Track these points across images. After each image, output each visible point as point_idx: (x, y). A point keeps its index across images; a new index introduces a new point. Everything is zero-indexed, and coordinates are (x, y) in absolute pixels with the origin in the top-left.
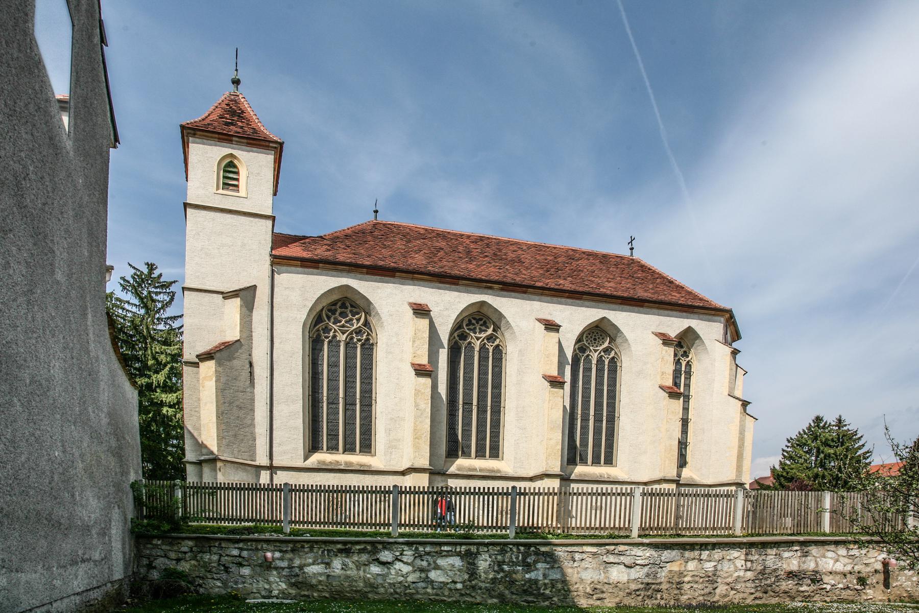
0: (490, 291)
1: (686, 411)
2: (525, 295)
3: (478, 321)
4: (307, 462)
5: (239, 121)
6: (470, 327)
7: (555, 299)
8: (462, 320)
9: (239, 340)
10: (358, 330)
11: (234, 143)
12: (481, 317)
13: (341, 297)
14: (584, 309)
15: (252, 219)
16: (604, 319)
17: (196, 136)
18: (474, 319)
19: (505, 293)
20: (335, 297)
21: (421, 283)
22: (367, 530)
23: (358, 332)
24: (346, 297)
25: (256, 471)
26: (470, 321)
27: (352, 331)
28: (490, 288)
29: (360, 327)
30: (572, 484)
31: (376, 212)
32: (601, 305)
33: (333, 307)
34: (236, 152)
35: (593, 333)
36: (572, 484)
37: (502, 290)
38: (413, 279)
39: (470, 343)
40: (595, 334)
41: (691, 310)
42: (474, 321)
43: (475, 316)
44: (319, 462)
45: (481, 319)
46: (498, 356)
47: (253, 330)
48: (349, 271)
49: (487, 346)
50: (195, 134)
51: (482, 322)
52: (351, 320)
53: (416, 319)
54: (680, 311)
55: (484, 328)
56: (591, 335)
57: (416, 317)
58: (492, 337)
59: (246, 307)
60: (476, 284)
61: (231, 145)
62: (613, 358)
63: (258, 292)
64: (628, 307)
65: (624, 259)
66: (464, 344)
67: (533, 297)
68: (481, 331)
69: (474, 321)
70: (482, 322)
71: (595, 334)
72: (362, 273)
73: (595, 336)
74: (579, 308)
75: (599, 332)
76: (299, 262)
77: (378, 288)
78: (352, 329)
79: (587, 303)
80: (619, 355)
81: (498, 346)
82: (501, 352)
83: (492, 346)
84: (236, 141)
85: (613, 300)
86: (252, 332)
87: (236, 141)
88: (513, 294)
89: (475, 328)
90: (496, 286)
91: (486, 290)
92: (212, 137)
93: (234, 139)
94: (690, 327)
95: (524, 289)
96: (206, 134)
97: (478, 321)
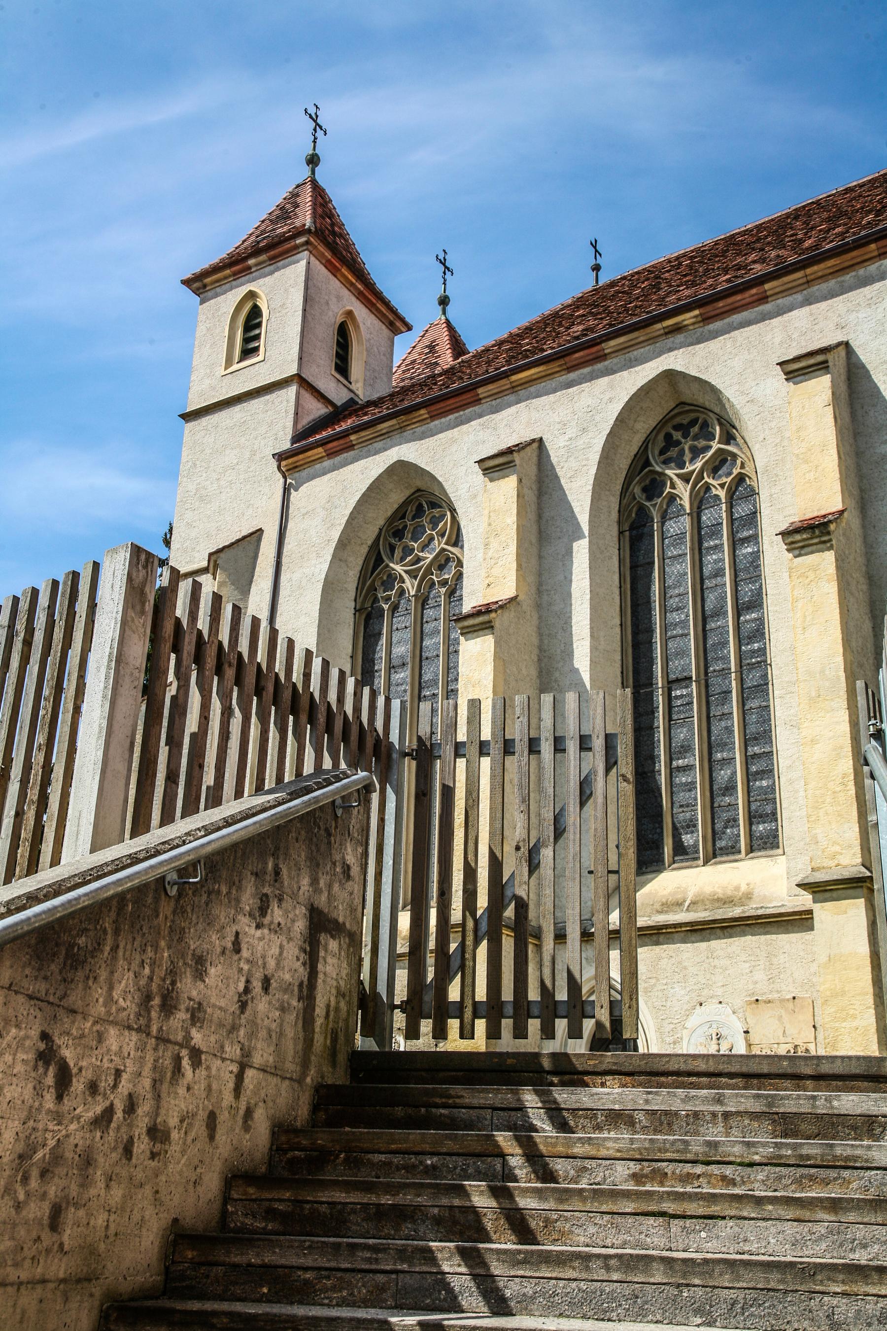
0: (680, 338)
1: (470, 887)
3: (684, 429)
9: (516, 597)
12: (693, 415)
13: (408, 493)
15: (267, 397)
18: (677, 428)
19: (717, 325)
22: (443, 1047)
26: (668, 437)
28: (678, 329)
30: (863, 900)
36: (863, 900)
37: (706, 319)
38: (514, 389)
42: (677, 435)
43: (678, 420)
45: (694, 422)
50: (205, 286)
51: (696, 429)
53: (490, 485)
55: (702, 443)
57: (491, 480)
58: (724, 461)
59: (233, 584)
61: (251, 276)
63: (265, 536)
68: (696, 453)
69: (677, 435)
76: (320, 450)
77: (454, 441)
78: (428, 561)
84: (256, 265)
89: (682, 453)
90: (688, 318)
91: (670, 341)
95: (754, 291)
97: (684, 429)
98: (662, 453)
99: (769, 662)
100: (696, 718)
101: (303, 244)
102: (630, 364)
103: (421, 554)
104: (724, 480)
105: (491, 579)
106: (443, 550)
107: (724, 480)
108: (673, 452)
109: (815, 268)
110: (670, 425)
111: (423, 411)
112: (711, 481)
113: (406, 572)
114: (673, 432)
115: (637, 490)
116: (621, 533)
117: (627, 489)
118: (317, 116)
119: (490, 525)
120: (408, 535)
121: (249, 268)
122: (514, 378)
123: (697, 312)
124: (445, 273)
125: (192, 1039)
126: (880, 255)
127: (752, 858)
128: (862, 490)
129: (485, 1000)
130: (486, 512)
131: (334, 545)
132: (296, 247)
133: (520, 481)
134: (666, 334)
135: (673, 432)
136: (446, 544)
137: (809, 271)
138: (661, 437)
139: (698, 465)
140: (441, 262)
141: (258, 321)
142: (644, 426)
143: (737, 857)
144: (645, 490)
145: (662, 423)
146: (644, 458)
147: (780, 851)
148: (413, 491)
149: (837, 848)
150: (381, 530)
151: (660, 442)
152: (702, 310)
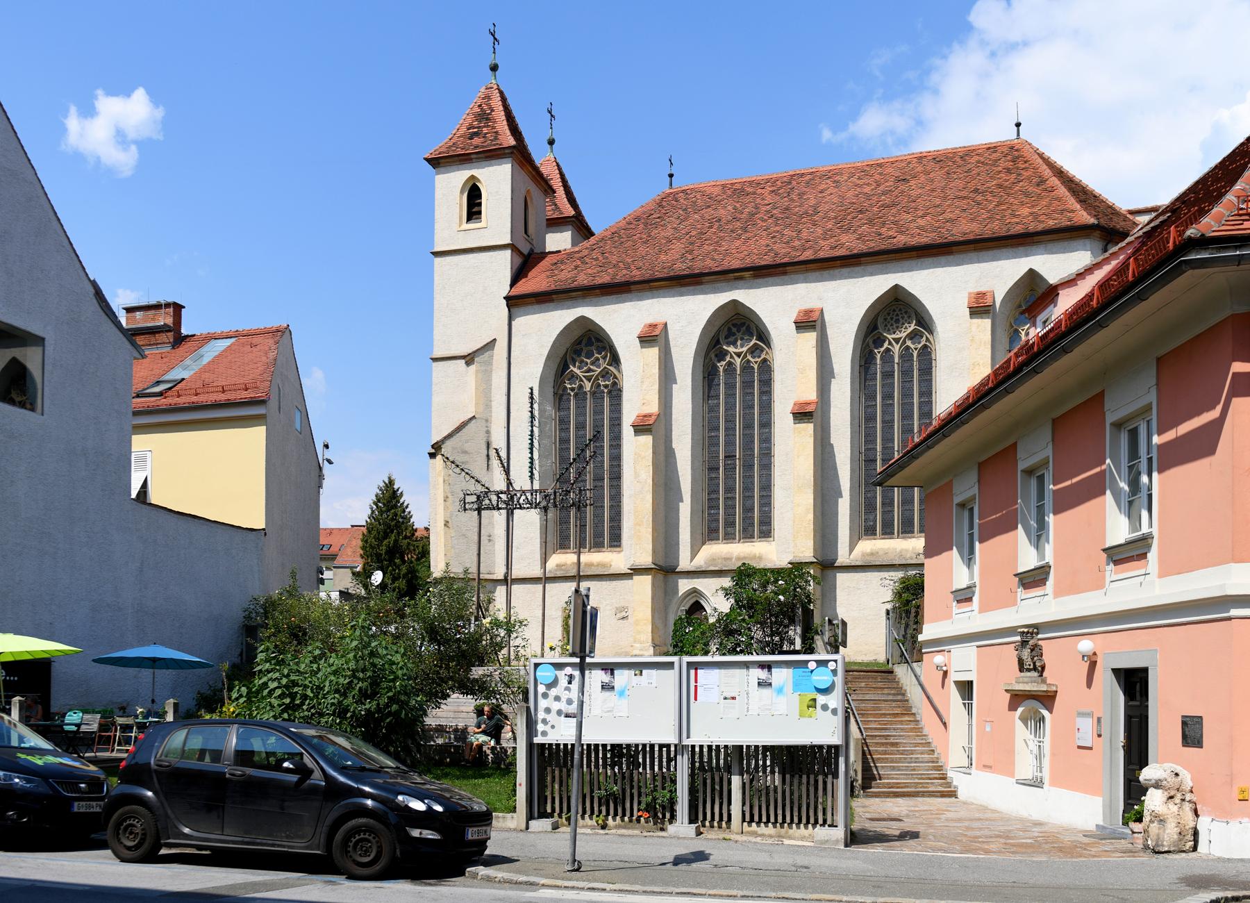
0: (741, 283)
2: (786, 278)
4: (851, 557)
5: (485, 127)
6: (730, 339)
7: (825, 273)
8: (719, 331)
10: (604, 373)
11: (474, 160)
12: (743, 321)
14: (867, 279)
16: (896, 287)
17: (441, 165)
18: (734, 325)
20: (577, 334)
21: (661, 291)
23: (605, 374)
24: (590, 330)
25: (666, 583)
26: (729, 329)
27: (597, 376)
28: (741, 278)
29: (605, 368)
31: (1018, 125)
32: (890, 265)
33: (578, 347)
34: (476, 172)
35: (894, 311)
37: (756, 277)
39: (730, 364)
40: (897, 312)
41: (1028, 240)
42: (734, 330)
43: (734, 322)
44: (713, 560)
45: (743, 324)
46: (766, 377)
47: (492, 399)
48: (584, 297)
49: (752, 365)
51: (744, 328)
52: (598, 359)
54: (1012, 246)
56: (900, 316)
60: (722, 277)
62: (925, 346)
64: (930, 260)
65: (996, 152)
66: (721, 365)
67: (796, 276)
69: (734, 330)
70: (744, 328)
71: (897, 312)
72: (597, 295)
73: (897, 315)
74: (860, 279)
75: (902, 307)
78: (597, 372)
79: (870, 268)
80: (932, 342)
81: (765, 360)
82: (770, 367)
83: (756, 362)
84: (476, 158)
85: (904, 254)
86: (491, 401)
87: (476, 158)
88: (770, 279)
90: (747, 274)
92: (453, 162)
93: (473, 156)
94: (1031, 270)
95: (781, 269)
96: (447, 160)
98: (726, 338)
99: (773, 454)
100: (737, 476)
101: (508, 153)
102: (715, 291)
103: (592, 367)
104: (757, 360)
105: (645, 401)
106: (605, 368)
107: (757, 360)
108: (731, 339)
109: (811, 265)
110: (731, 323)
111: (597, 291)
112: (751, 359)
113: (584, 376)
114: (732, 328)
115: (713, 356)
116: (704, 378)
117: (708, 355)
118: (495, 32)
119: (644, 372)
120: (583, 354)
121: (471, 159)
122: (652, 284)
123: (751, 273)
124: (494, 44)
125: (1145, 796)
126: (841, 266)
127: (760, 541)
128: (822, 385)
129: (1101, 798)
130: (642, 364)
131: (545, 358)
132: (505, 154)
133: (659, 349)
134: (735, 279)
135: (732, 328)
136: (607, 365)
137: (808, 266)
138: (726, 329)
139: (745, 349)
140: (492, 34)
141: (479, 201)
142: (718, 323)
143: (753, 540)
144: (716, 356)
145: (727, 322)
146: (717, 338)
147: (772, 539)
148: (586, 330)
149: (804, 549)
150: (568, 349)
151: (725, 332)
152: (755, 272)
